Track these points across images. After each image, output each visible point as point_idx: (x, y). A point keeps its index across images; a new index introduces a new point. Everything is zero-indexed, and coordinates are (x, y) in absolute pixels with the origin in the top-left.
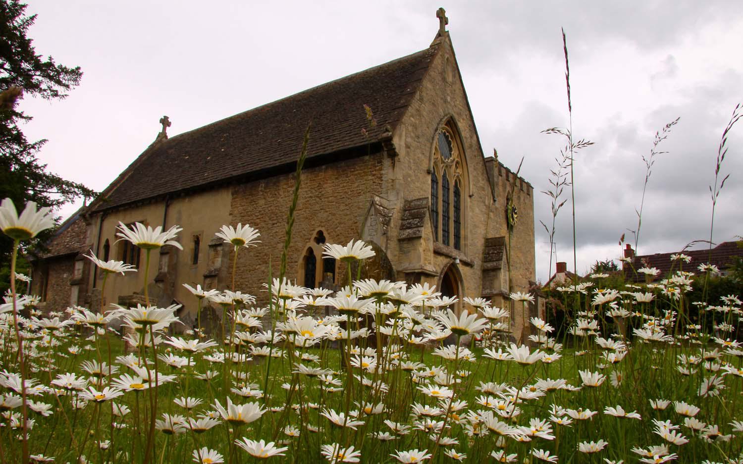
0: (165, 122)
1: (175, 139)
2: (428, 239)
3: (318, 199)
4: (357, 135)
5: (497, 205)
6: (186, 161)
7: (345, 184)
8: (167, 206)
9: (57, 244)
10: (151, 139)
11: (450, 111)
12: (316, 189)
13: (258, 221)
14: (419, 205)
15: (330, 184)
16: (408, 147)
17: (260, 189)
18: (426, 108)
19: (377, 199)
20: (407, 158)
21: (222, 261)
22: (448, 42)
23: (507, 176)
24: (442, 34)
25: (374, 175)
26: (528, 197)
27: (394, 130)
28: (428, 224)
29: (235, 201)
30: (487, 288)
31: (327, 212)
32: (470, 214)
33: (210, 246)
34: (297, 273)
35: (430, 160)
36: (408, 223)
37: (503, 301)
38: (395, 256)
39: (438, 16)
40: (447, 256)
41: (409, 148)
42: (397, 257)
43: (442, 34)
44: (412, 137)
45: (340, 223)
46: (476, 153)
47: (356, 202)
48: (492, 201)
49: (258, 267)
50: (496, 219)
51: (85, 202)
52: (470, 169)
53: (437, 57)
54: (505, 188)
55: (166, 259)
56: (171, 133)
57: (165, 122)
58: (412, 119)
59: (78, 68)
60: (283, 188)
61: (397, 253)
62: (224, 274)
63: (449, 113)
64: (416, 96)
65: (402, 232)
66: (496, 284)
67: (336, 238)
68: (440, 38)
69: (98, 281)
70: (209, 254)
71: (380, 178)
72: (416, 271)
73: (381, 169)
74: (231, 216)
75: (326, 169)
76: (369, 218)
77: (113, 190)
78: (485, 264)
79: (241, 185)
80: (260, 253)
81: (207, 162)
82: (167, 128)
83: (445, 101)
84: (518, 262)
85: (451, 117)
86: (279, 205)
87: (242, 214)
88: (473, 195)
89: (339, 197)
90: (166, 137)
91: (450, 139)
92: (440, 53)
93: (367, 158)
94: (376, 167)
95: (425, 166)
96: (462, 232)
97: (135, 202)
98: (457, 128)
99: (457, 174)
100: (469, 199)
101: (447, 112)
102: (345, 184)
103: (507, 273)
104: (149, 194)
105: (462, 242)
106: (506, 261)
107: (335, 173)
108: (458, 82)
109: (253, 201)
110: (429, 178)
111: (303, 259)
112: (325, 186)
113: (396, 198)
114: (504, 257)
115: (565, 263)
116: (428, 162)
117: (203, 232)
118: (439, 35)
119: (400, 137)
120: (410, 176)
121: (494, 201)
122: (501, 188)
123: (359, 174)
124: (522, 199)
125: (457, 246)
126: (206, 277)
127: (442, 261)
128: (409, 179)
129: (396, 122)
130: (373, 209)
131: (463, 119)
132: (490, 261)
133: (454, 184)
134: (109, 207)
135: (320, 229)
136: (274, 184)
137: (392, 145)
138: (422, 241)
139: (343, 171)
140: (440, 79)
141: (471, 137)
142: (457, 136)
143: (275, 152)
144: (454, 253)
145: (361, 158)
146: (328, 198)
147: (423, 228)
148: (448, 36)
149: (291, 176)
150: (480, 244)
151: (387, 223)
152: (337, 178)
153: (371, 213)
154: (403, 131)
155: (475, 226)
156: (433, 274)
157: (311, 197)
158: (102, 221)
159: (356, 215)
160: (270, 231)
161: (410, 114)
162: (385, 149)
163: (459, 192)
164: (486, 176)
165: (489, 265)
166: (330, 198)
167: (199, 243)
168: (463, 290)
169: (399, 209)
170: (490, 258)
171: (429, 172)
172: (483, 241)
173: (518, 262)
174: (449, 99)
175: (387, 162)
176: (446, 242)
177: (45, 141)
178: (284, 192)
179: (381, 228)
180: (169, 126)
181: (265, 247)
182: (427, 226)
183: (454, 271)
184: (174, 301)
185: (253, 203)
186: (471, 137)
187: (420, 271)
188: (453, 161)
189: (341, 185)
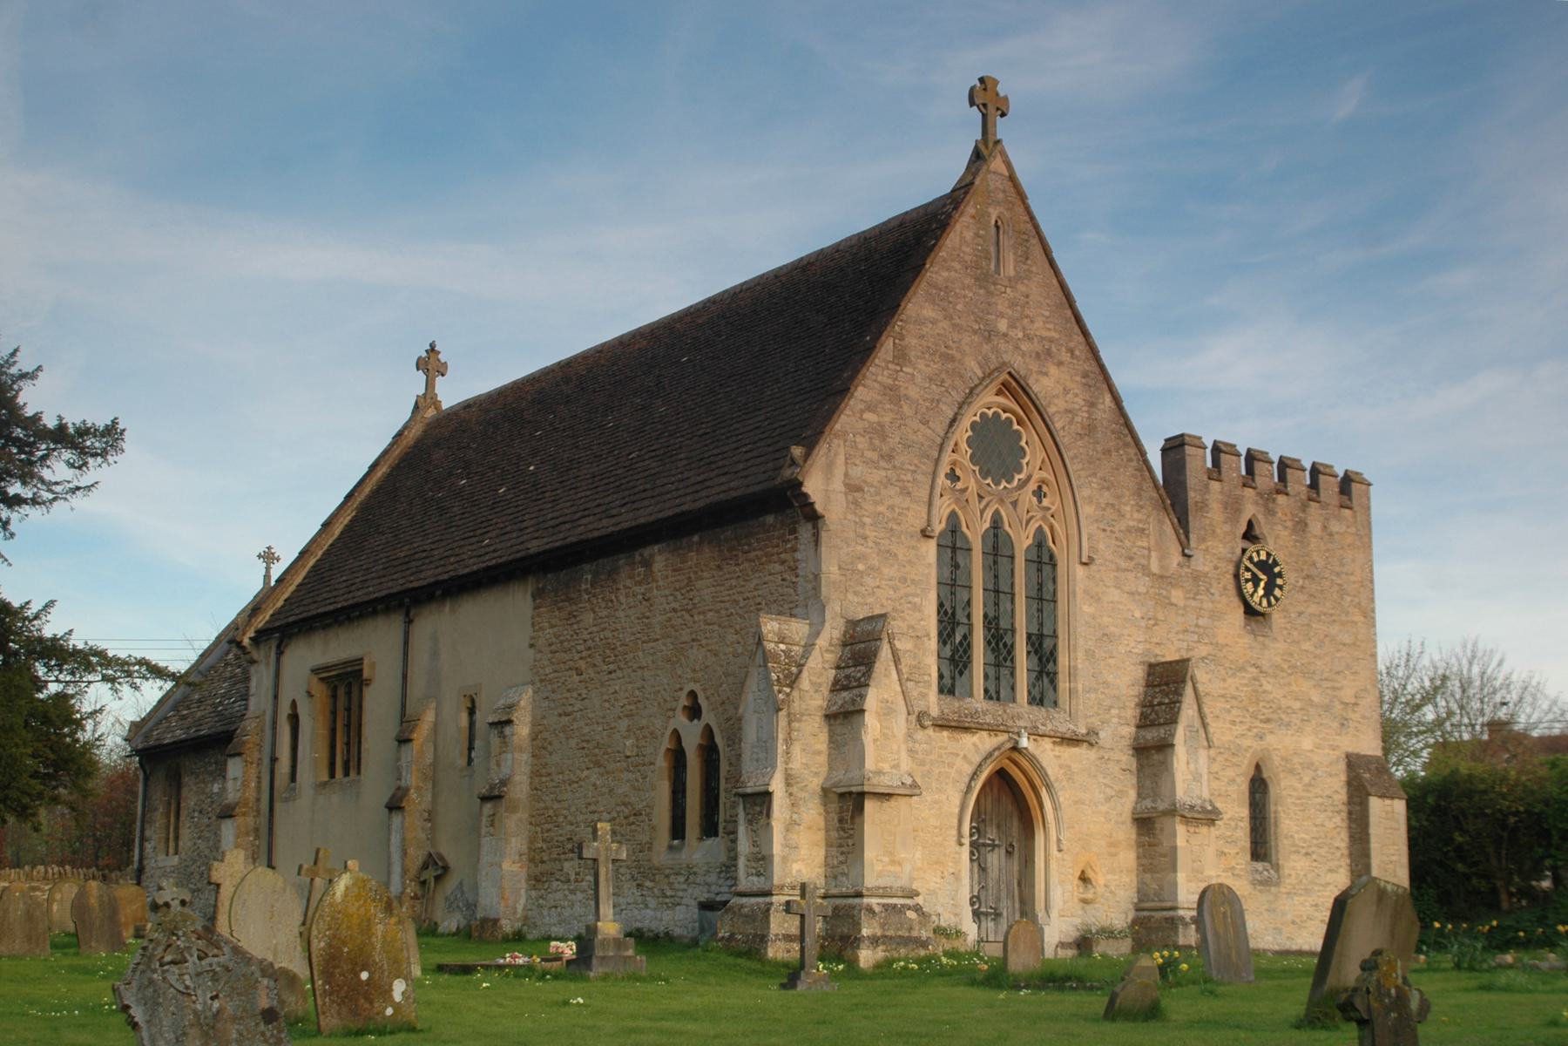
0: (431, 364)
3: (687, 616)
5: (1201, 563)
7: (734, 582)
8: (409, 622)
9: (200, 701)
10: (400, 415)
11: (1006, 358)
14: (869, 633)
16: (853, 488)
18: (922, 368)
20: (850, 517)
26: (1347, 511)
28: (887, 676)
32: (1085, 609)
34: (653, 788)
36: (847, 677)
40: (993, 730)
41: (859, 489)
48: (1176, 558)
49: (586, 773)
50: (1194, 603)
51: (267, 576)
56: (451, 394)
57: (431, 364)
58: (867, 415)
59: (114, 422)
60: (626, 587)
69: (278, 806)
71: (794, 569)
73: (794, 550)
74: (532, 651)
75: (700, 543)
78: (1143, 732)
82: (439, 379)
83: (989, 335)
93: (770, 519)
97: (343, 608)
100: (1080, 571)
101: (994, 364)
102: (734, 582)
104: (374, 591)
109: (571, 615)
112: (699, 584)
119: (830, 467)
123: (759, 558)
124: (1315, 527)
127: (979, 744)
132: (1153, 725)
134: (291, 619)
137: (806, 496)
146: (704, 613)
154: (836, 454)
157: (674, 610)
158: (280, 653)
165: (1150, 735)
166: (710, 614)
170: (1153, 716)
172: (1140, 673)
174: (1002, 325)
177: (53, 602)
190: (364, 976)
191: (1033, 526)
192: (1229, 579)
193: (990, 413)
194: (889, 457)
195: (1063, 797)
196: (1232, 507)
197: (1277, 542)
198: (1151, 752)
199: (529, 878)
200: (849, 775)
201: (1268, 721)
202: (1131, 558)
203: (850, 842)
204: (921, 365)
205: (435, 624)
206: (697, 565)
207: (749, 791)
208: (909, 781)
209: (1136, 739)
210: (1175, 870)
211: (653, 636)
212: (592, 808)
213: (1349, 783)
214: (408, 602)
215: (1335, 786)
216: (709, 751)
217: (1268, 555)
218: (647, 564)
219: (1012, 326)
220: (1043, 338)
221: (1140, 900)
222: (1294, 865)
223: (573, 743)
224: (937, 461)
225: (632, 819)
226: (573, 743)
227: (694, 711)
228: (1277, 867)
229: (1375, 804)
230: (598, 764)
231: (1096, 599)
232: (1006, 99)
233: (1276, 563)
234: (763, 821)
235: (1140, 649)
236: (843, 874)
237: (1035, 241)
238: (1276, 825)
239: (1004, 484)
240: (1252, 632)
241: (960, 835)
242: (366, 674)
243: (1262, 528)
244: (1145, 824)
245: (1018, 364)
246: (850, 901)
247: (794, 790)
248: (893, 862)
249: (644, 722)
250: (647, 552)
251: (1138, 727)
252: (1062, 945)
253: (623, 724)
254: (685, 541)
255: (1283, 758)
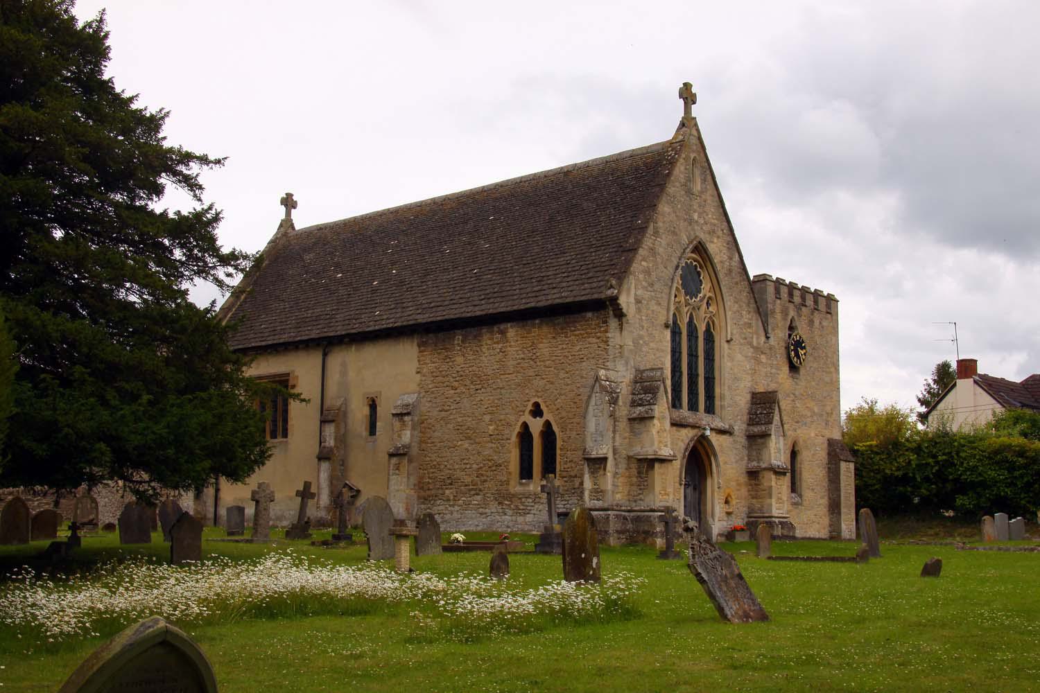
0: (289, 202)
1: (309, 233)
2: (664, 418)
3: (532, 362)
4: (577, 283)
5: (772, 341)
6: (340, 281)
8: (325, 355)
11: (697, 234)
12: (529, 349)
13: (456, 384)
14: (652, 377)
15: (547, 343)
16: (638, 301)
17: (456, 342)
18: (663, 241)
19: (602, 373)
21: (412, 435)
22: (696, 134)
23: (791, 295)
24: (688, 123)
25: (599, 338)
26: (829, 316)
27: (620, 287)
29: (423, 356)
30: (754, 460)
31: (543, 379)
33: (394, 415)
35: (668, 310)
36: (640, 399)
37: (773, 477)
38: (625, 438)
39: (681, 97)
40: (693, 427)
41: (640, 302)
42: (627, 440)
43: (688, 123)
44: (645, 288)
45: (561, 395)
46: (738, 279)
47: (577, 370)
48: (763, 339)
50: (770, 362)
52: (728, 304)
53: (678, 164)
54: (787, 315)
55: (330, 430)
56: (303, 220)
57: (289, 202)
58: (643, 263)
61: (627, 435)
62: (415, 451)
63: (696, 237)
64: (649, 232)
65: (633, 410)
66: (765, 456)
67: (556, 413)
68: (684, 129)
70: (392, 425)
71: (606, 342)
72: (649, 457)
73: (606, 331)
74: (419, 375)
75: (541, 324)
76: (594, 395)
77: (227, 318)
78: (751, 428)
79: (431, 335)
80: (461, 426)
81: (374, 291)
82: (293, 210)
83: (691, 222)
84: (809, 414)
85: (700, 242)
86: (483, 365)
87: (434, 374)
88: (732, 340)
89: (557, 361)
90: (292, 226)
91: (699, 269)
92: (684, 156)
93: (589, 315)
94: (601, 327)
95: (662, 319)
96: (717, 391)
98: (708, 255)
99: (708, 315)
100: (726, 345)
103: (781, 438)
105: (717, 403)
106: (779, 424)
107: (552, 331)
108: (710, 187)
110: (668, 334)
111: (517, 435)
112: (541, 346)
113: (625, 369)
114: (777, 418)
115: (975, 361)
116: (665, 313)
117: (381, 392)
118: (683, 125)
119: (629, 290)
120: (641, 337)
121: (768, 338)
122: (779, 316)
123: (581, 334)
125: (710, 409)
126: (391, 455)
127: (687, 435)
128: (641, 342)
129: (622, 274)
130: (597, 385)
131: (718, 237)
132: (757, 424)
133: (704, 329)
135: (537, 400)
136: (475, 337)
137: (619, 305)
138: (656, 421)
139: (562, 329)
140: (683, 193)
141: (731, 258)
142: (709, 264)
143: (471, 290)
144: (703, 418)
145: (583, 314)
146: (544, 361)
147: (656, 406)
148: (696, 125)
149: (496, 329)
150: (743, 401)
151: (614, 401)
152: (554, 338)
153: (595, 391)
155: (736, 379)
156: (670, 458)
157: (523, 359)
159: (578, 385)
160: (472, 398)
161: (640, 258)
162: (611, 309)
163: (713, 337)
164: (755, 306)
167: (376, 407)
168: (718, 466)
169: (628, 382)
170: (757, 420)
171: (667, 326)
172: (748, 397)
173: (809, 414)
174: (696, 216)
175: (613, 323)
176: (693, 406)
178: (488, 349)
179: (608, 409)
180: (295, 208)
181: (467, 418)
182: (661, 402)
183: (705, 443)
184: (346, 484)
185: (448, 360)
186: (731, 258)
187: (653, 457)
188: (701, 300)
189: (561, 347)
190: (583, 555)
191: (706, 321)
192: (783, 351)
193: (689, 262)
194: (652, 285)
195: (721, 459)
196: (785, 313)
197: (802, 331)
198: (756, 439)
199: (419, 498)
200: (645, 450)
201: (797, 422)
202: (746, 339)
203: (646, 483)
204: (664, 236)
205: (337, 359)
206: (539, 335)
207: (593, 456)
208: (672, 453)
209: (746, 431)
210: (771, 498)
211: (508, 372)
212: (465, 461)
213: (829, 454)
214: (326, 344)
215: (822, 454)
216: (548, 434)
217: (800, 337)
218: (503, 333)
219: (699, 217)
220: (711, 224)
221: (750, 513)
222: (808, 495)
223: (451, 426)
224: (671, 287)
225: (494, 468)
226: (451, 426)
227: (537, 412)
228: (800, 496)
229: (843, 465)
230: (469, 438)
231: (732, 359)
232: (695, 94)
233: (803, 342)
234: (601, 472)
235: (749, 385)
236: (641, 500)
237: (708, 172)
238: (801, 474)
239: (694, 299)
240: (792, 377)
241: (681, 480)
242: (291, 383)
243: (797, 323)
244: (753, 474)
245: (702, 236)
246: (646, 513)
247: (616, 457)
248: (665, 494)
249: (502, 417)
250: (502, 327)
251: (748, 425)
252: (720, 535)
253: (487, 418)
254: (529, 322)
255: (804, 441)
